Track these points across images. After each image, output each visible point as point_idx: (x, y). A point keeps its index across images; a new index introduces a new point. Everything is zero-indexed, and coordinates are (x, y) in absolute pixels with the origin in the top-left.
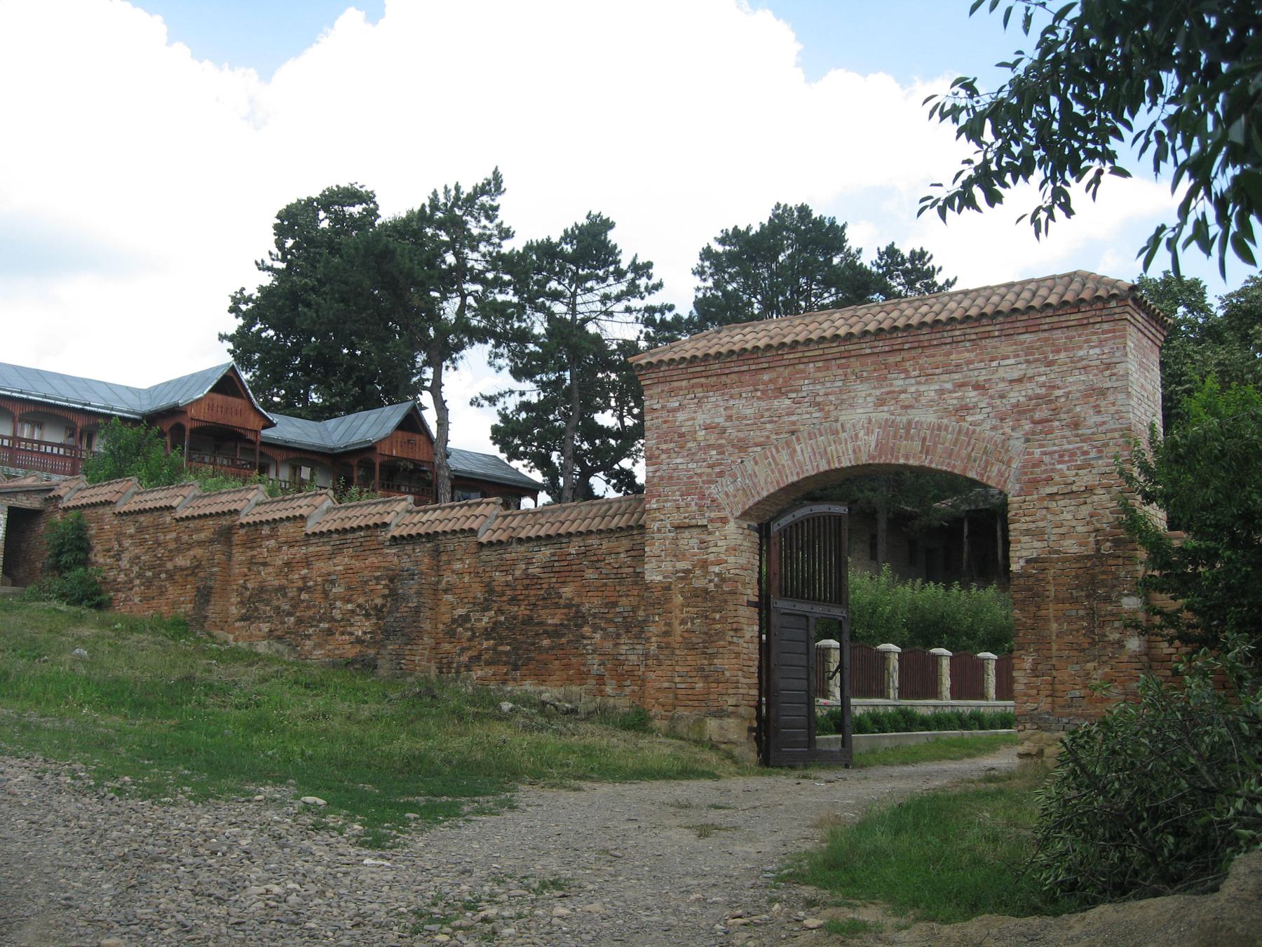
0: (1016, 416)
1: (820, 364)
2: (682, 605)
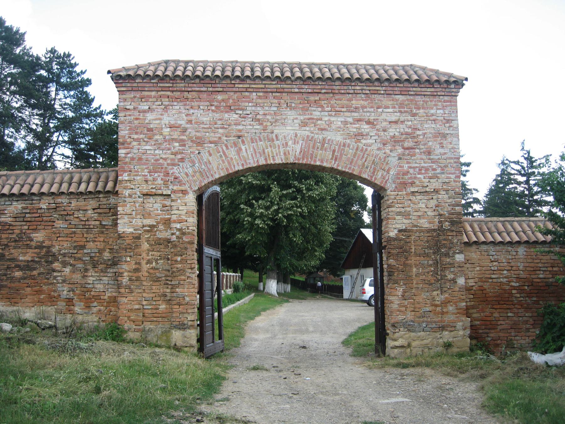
0: (393, 143)
1: (261, 94)
2: (148, 250)
